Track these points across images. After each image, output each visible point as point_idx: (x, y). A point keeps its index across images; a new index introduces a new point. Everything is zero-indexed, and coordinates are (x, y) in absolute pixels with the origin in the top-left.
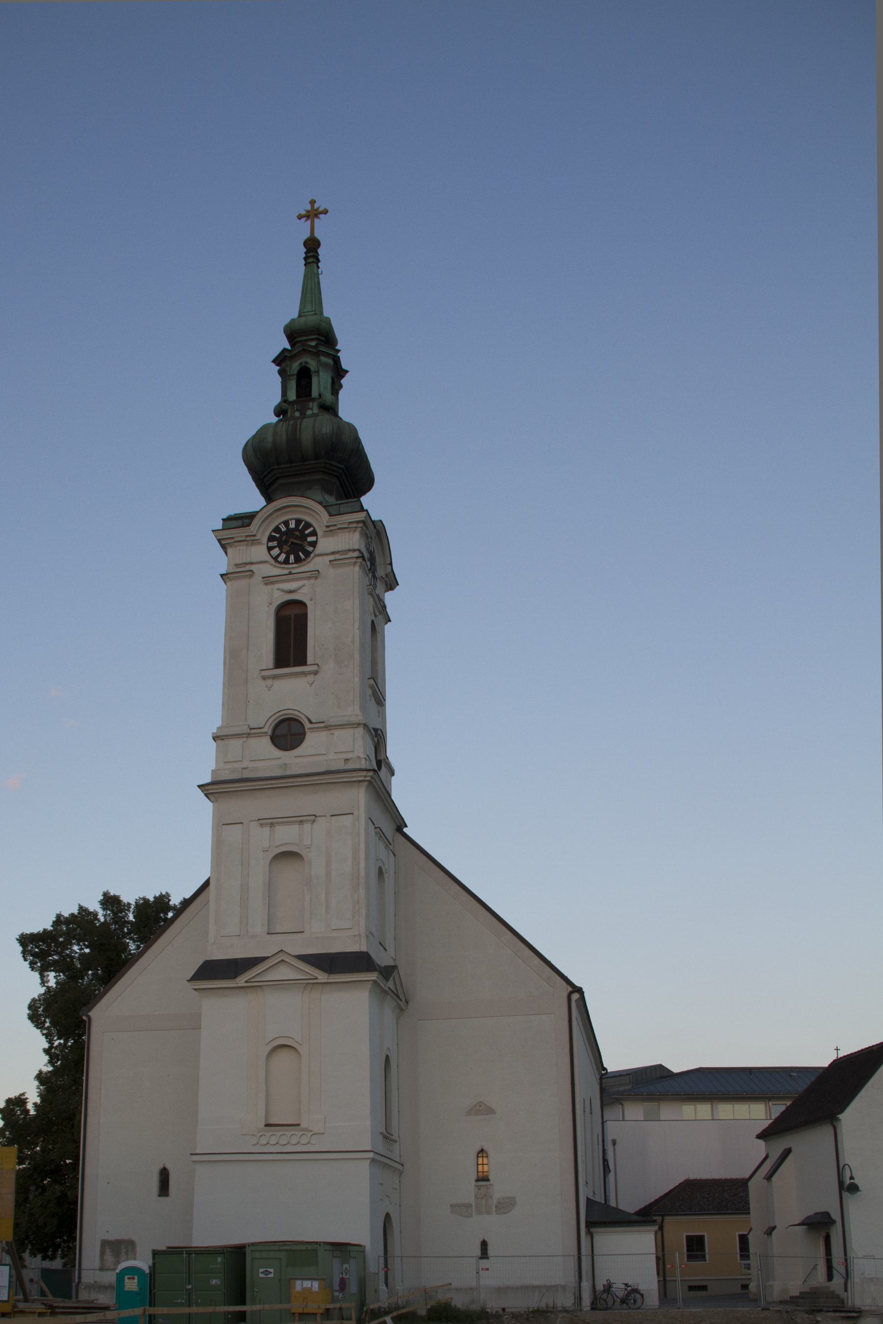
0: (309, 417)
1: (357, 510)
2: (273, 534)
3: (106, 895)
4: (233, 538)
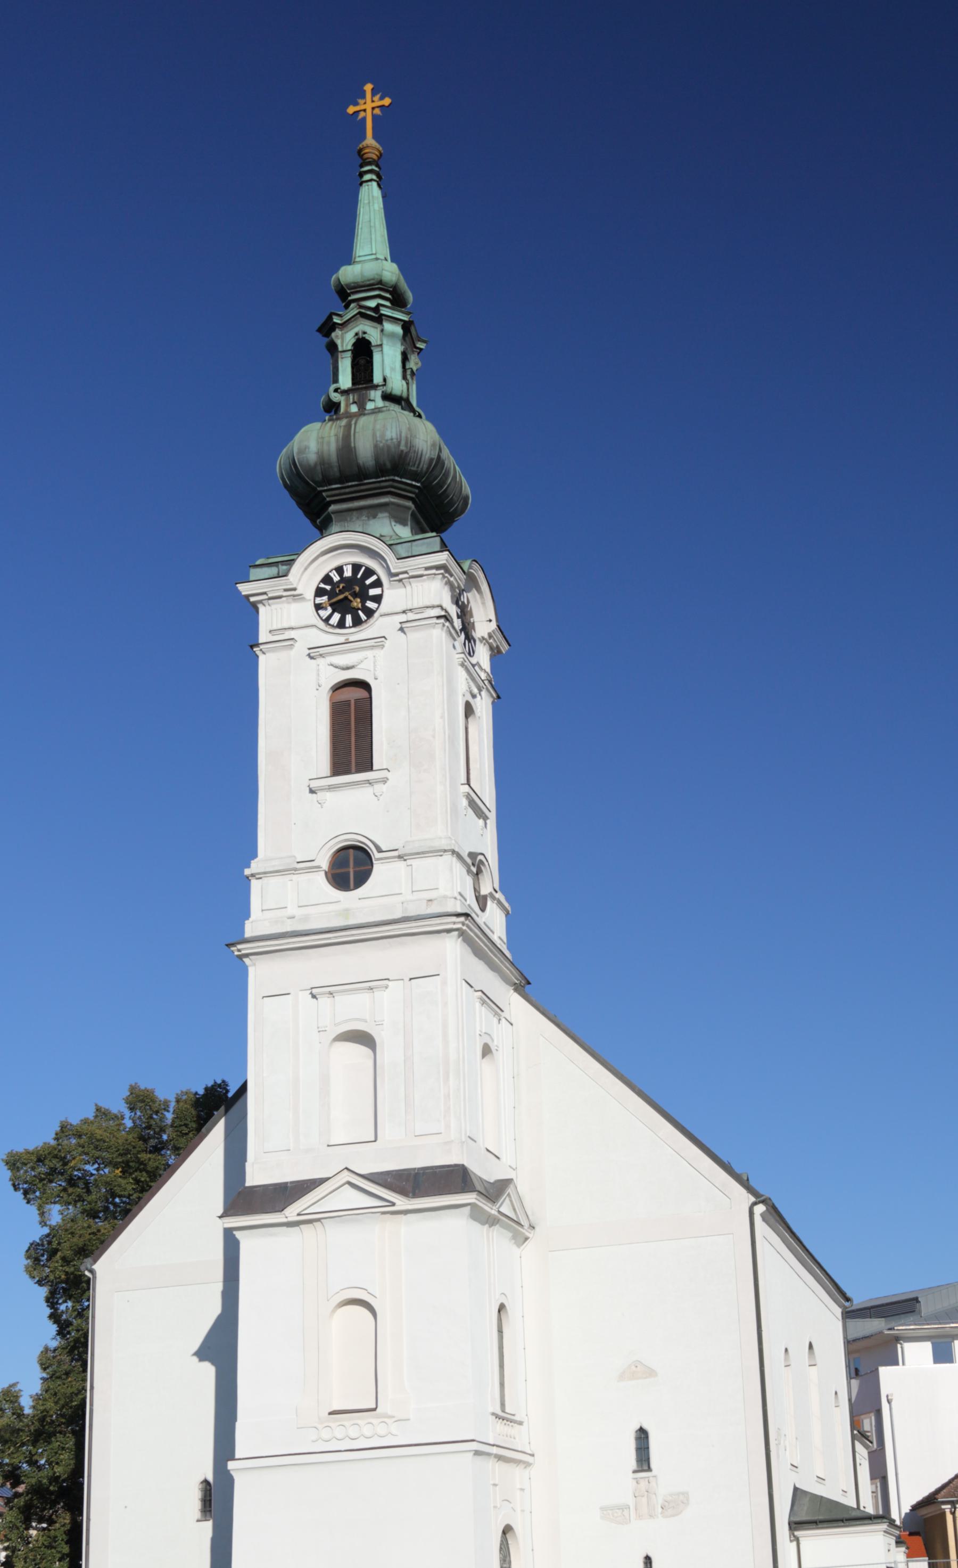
0: (369, 414)
1: (436, 550)
2: (322, 585)
3: (133, 1089)
4: (265, 593)
